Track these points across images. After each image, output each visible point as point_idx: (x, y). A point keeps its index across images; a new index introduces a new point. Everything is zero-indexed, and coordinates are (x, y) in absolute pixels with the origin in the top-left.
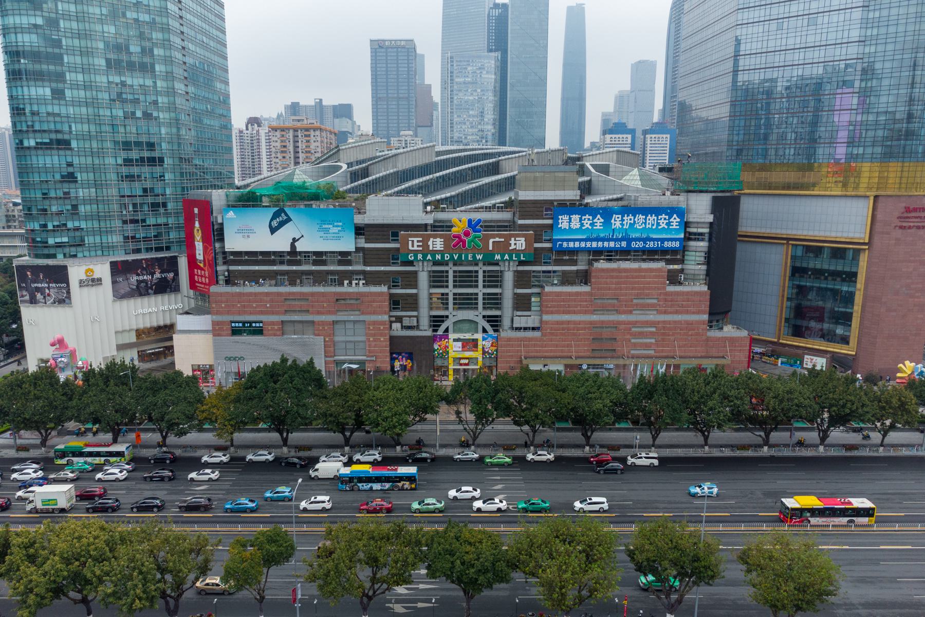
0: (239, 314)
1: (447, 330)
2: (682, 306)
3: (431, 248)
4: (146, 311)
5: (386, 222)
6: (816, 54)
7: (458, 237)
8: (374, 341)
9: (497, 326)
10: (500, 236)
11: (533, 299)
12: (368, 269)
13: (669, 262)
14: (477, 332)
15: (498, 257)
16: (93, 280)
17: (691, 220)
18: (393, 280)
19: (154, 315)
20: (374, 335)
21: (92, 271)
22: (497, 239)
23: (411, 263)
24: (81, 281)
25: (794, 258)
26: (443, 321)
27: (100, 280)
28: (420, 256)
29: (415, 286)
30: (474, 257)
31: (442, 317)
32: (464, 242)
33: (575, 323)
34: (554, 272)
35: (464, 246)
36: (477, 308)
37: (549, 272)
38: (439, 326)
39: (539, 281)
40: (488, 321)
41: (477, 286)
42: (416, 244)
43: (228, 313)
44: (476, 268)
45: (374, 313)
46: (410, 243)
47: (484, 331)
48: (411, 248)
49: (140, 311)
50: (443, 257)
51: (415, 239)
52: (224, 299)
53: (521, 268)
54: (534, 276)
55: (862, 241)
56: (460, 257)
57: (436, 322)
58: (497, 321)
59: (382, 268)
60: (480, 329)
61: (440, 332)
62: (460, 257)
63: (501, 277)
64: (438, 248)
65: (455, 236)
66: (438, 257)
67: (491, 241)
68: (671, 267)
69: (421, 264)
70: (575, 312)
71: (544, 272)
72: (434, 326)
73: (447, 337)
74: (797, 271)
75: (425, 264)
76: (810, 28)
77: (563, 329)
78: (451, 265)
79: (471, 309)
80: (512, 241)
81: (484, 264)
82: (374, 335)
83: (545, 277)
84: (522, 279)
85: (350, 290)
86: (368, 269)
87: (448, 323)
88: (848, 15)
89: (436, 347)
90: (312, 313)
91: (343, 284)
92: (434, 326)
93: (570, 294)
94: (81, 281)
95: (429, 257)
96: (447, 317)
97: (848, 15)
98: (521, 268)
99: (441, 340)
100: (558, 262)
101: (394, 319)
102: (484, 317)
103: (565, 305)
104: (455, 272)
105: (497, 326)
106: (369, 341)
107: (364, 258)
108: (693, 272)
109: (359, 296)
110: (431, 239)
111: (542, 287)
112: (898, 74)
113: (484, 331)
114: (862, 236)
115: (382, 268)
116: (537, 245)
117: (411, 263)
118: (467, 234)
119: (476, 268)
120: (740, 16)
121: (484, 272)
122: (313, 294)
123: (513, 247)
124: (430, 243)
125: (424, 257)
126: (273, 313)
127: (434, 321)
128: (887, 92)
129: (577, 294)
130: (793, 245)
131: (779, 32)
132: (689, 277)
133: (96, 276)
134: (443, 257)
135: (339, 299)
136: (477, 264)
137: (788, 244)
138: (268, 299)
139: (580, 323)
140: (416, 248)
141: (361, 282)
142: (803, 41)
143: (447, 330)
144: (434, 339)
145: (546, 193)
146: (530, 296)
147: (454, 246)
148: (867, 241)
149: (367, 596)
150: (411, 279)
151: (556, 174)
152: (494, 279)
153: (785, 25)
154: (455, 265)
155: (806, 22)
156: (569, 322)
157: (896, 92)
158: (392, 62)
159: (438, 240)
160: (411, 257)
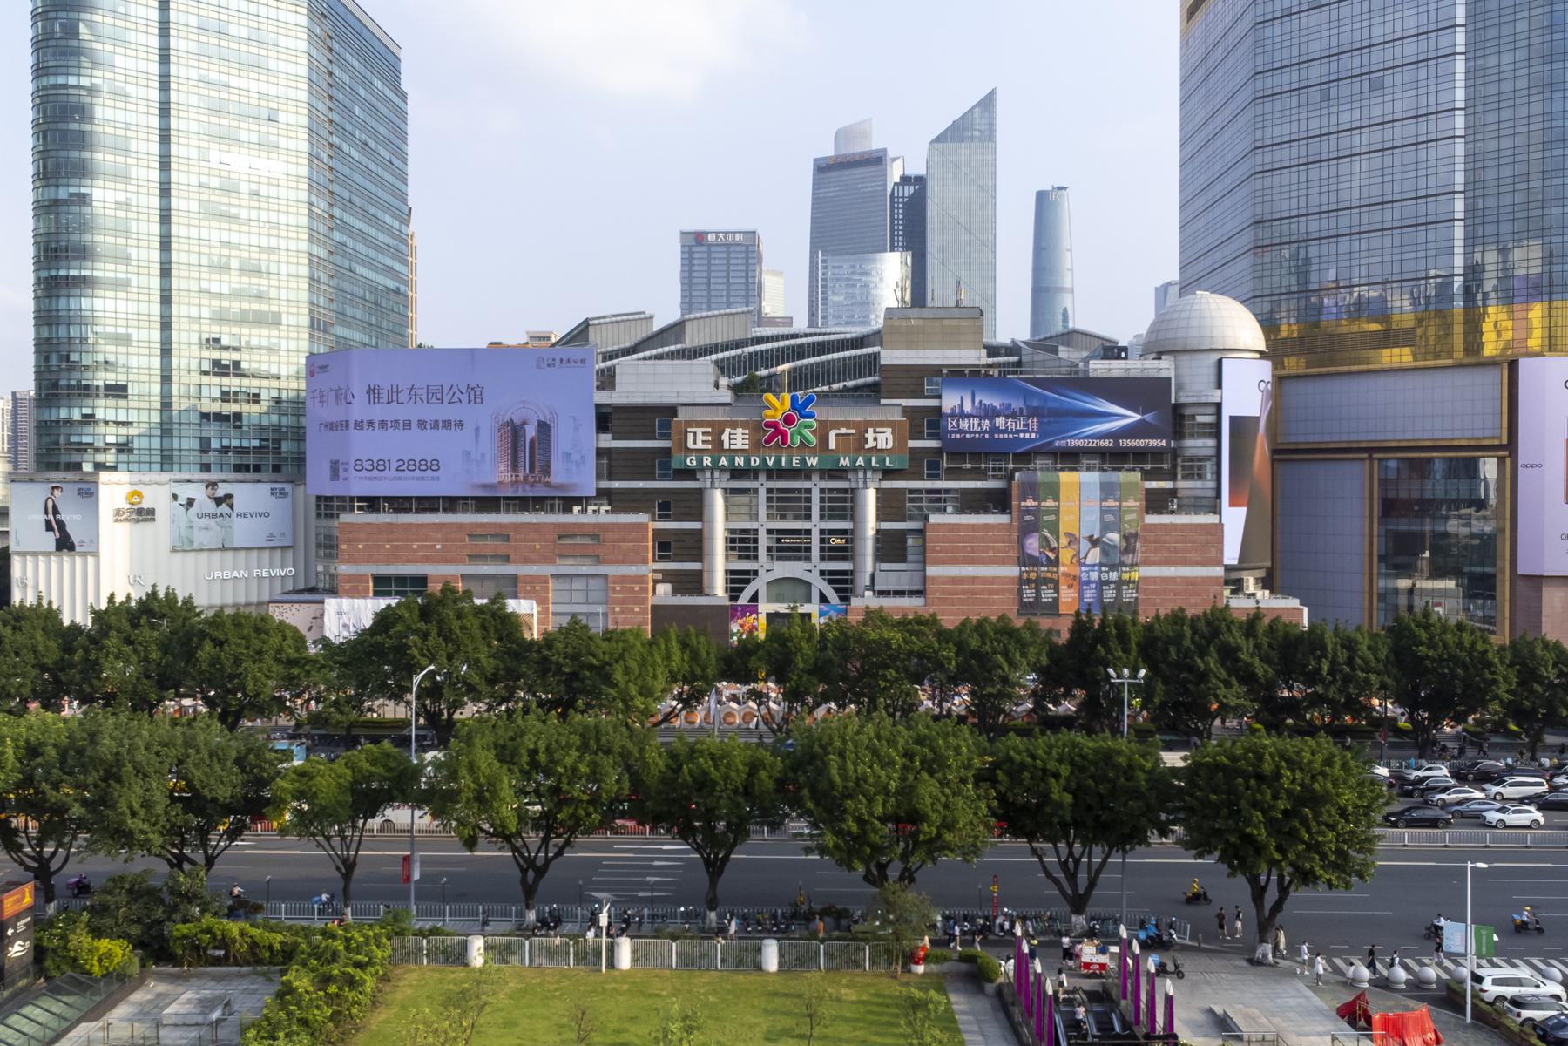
0: (388, 562)
1: (755, 598)
2: (1176, 551)
3: (726, 446)
4: (228, 574)
5: (649, 400)
6: (1388, 135)
7: (774, 425)
8: (622, 612)
9: (846, 590)
10: (847, 424)
11: (910, 541)
12: (616, 485)
13: (1147, 476)
14: (809, 601)
15: (845, 462)
16: (140, 511)
17: (1183, 400)
18: (664, 505)
19: (242, 585)
20: (622, 602)
21: (139, 494)
22: (843, 431)
23: (690, 474)
24: (118, 512)
25: (1384, 482)
26: (748, 582)
27: (151, 512)
28: (707, 461)
29: (699, 516)
30: (803, 461)
31: (747, 572)
32: (784, 435)
33: (985, 580)
34: (947, 491)
35: (784, 441)
36: (808, 559)
37: (938, 491)
38: (741, 590)
39: (920, 508)
40: (830, 582)
41: (808, 517)
42: (700, 437)
43: (369, 560)
44: (807, 485)
45: (622, 561)
46: (690, 437)
47: (823, 599)
48: (690, 445)
49: (218, 574)
50: (747, 461)
51: (699, 431)
52: (362, 534)
53: (887, 484)
54: (911, 500)
55: (1496, 442)
56: (778, 461)
57: (738, 581)
58: (845, 581)
59: (641, 484)
60: (815, 596)
61: (744, 600)
62: (778, 461)
63: (853, 500)
64: (739, 446)
65: (768, 425)
66: (740, 462)
67: (832, 434)
68: (1154, 485)
69: (708, 474)
70: (983, 562)
71: (929, 491)
72: (733, 590)
73: (755, 610)
74: (1390, 508)
75: (716, 474)
76: (1374, 94)
77: (964, 592)
78: (762, 477)
79: (798, 559)
80: (870, 435)
81: (822, 478)
82: (622, 602)
83: (931, 501)
84: (890, 505)
85: (584, 519)
86: (616, 485)
87: (758, 585)
88: (1432, 70)
89: (735, 627)
90: (515, 562)
91: (571, 511)
92: (733, 590)
93: (974, 527)
94: (118, 512)
95: (724, 462)
96: (756, 573)
97: (1432, 70)
98: (887, 484)
99: (743, 615)
100: (955, 474)
101: (659, 576)
102: (822, 573)
103: (968, 549)
104: (769, 491)
105: (846, 590)
106: (614, 612)
107: (610, 467)
108: (1189, 493)
109: (596, 534)
110: (727, 431)
111: (926, 518)
112: (1525, 157)
113: (823, 599)
114: (1497, 432)
115: (641, 484)
116: (912, 444)
117: (690, 474)
118: (789, 420)
119: (807, 485)
120: (1259, 84)
121: (822, 491)
122: (517, 527)
123: (871, 444)
124: (725, 437)
125: (715, 461)
126: (446, 561)
127: (733, 581)
128: (1510, 188)
129: (987, 527)
130: (1380, 460)
131: (1324, 104)
132: (1185, 502)
133: (145, 505)
134: (747, 461)
135: (564, 533)
136: (808, 478)
137: (1371, 459)
138: (439, 535)
139: (994, 580)
140: (699, 445)
141: (603, 509)
142: (1303, 51)
143: (755, 598)
144: (733, 612)
145: (929, 353)
146: (903, 534)
147: (768, 442)
148: (1505, 441)
149: (531, 862)
150: (694, 505)
151: (946, 322)
152: (843, 505)
153: (1333, 93)
154: (770, 477)
155: (1366, 85)
156: (973, 580)
157: (1524, 186)
158: (718, 263)
159: (740, 431)
160: (692, 462)
